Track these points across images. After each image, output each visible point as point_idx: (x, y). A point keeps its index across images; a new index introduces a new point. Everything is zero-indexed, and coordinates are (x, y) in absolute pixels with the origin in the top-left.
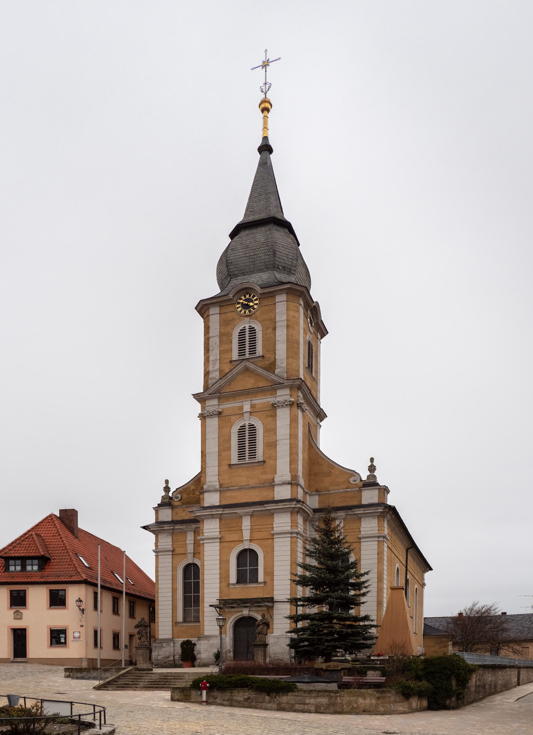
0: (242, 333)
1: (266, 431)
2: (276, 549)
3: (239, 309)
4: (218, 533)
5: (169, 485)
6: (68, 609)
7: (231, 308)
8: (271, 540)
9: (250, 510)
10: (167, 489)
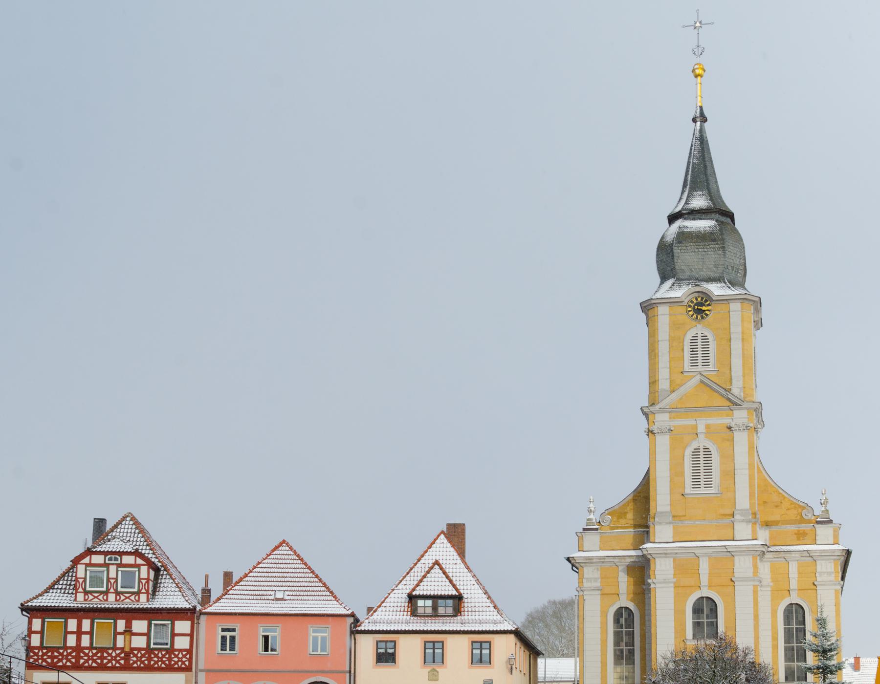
0: (695, 338)
4: (672, 576)
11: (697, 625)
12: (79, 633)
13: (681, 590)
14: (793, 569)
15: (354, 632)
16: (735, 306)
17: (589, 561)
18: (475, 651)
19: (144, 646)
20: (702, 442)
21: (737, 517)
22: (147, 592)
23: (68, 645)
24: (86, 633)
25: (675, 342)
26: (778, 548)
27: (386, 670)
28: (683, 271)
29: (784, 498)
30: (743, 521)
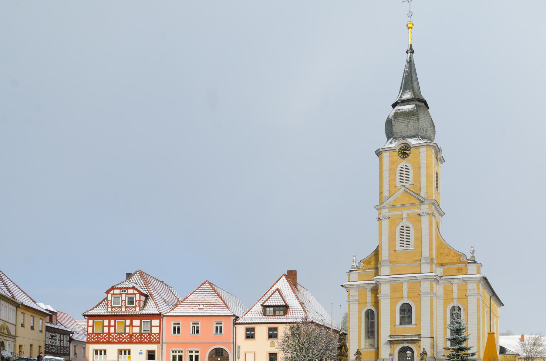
0: (402, 169)
11: (402, 318)
12: (109, 326)
13: (394, 300)
14: (455, 288)
15: (235, 324)
16: (423, 149)
17: (352, 286)
19: (138, 332)
20: (405, 223)
21: (422, 261)
22: (140, 306)
23: (105, 332)
24: (112, 326)
25: (392, 171)
26: (447, 277)
27: (250, 342)
28: (397, 133)
29: (451, 250)
30: (425, 263)
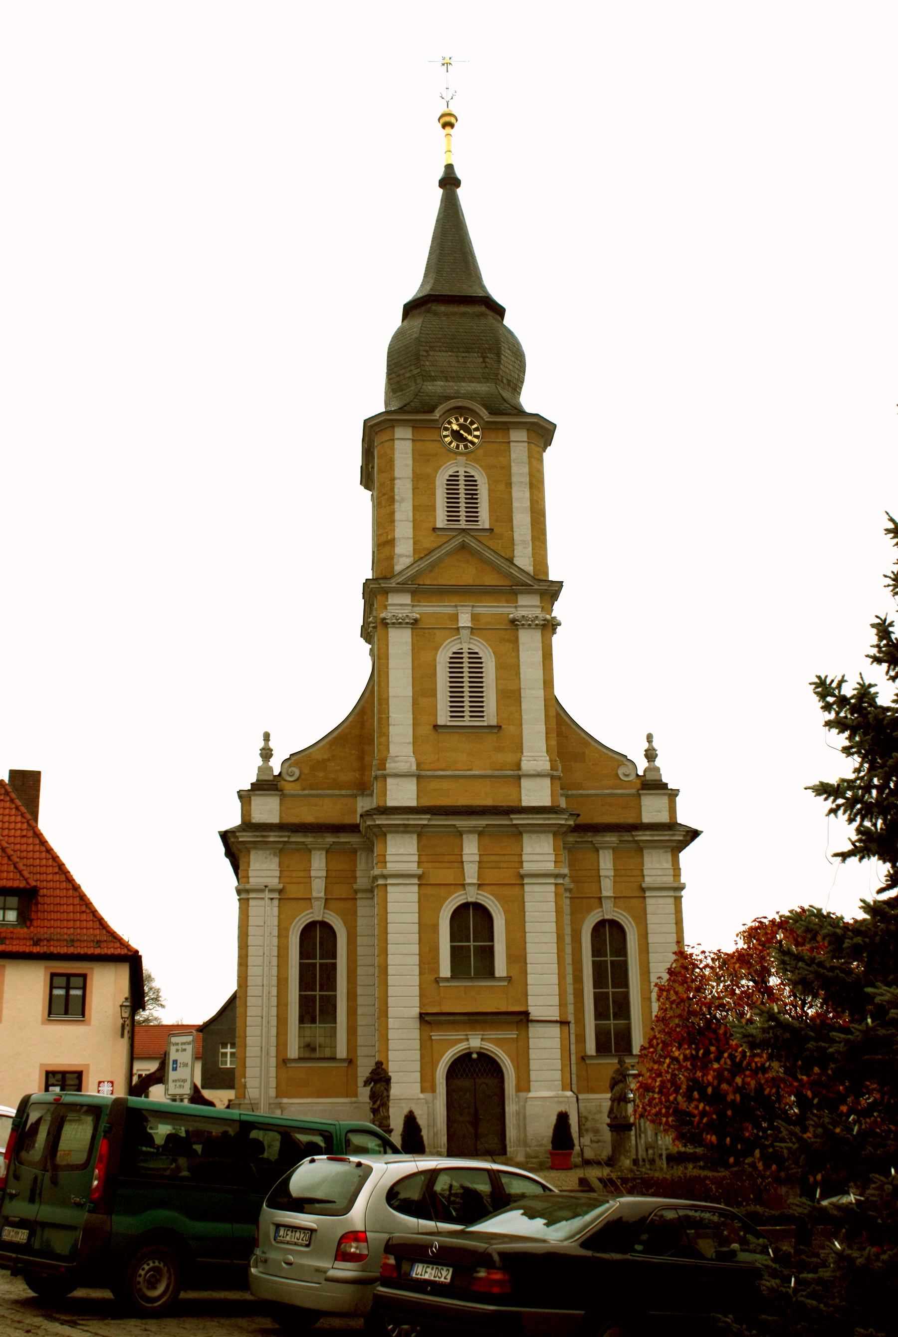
1: (500, 667)
2: (528, 906)
3: (448, 439)
4: (416, 865)
5: (271, 744)
6: (89, 1024)
7: (433, 435)
8: (517, 888)
9: (481, 822)
10: (266, 753)
18: (56, 992)
25: (422, 482)
